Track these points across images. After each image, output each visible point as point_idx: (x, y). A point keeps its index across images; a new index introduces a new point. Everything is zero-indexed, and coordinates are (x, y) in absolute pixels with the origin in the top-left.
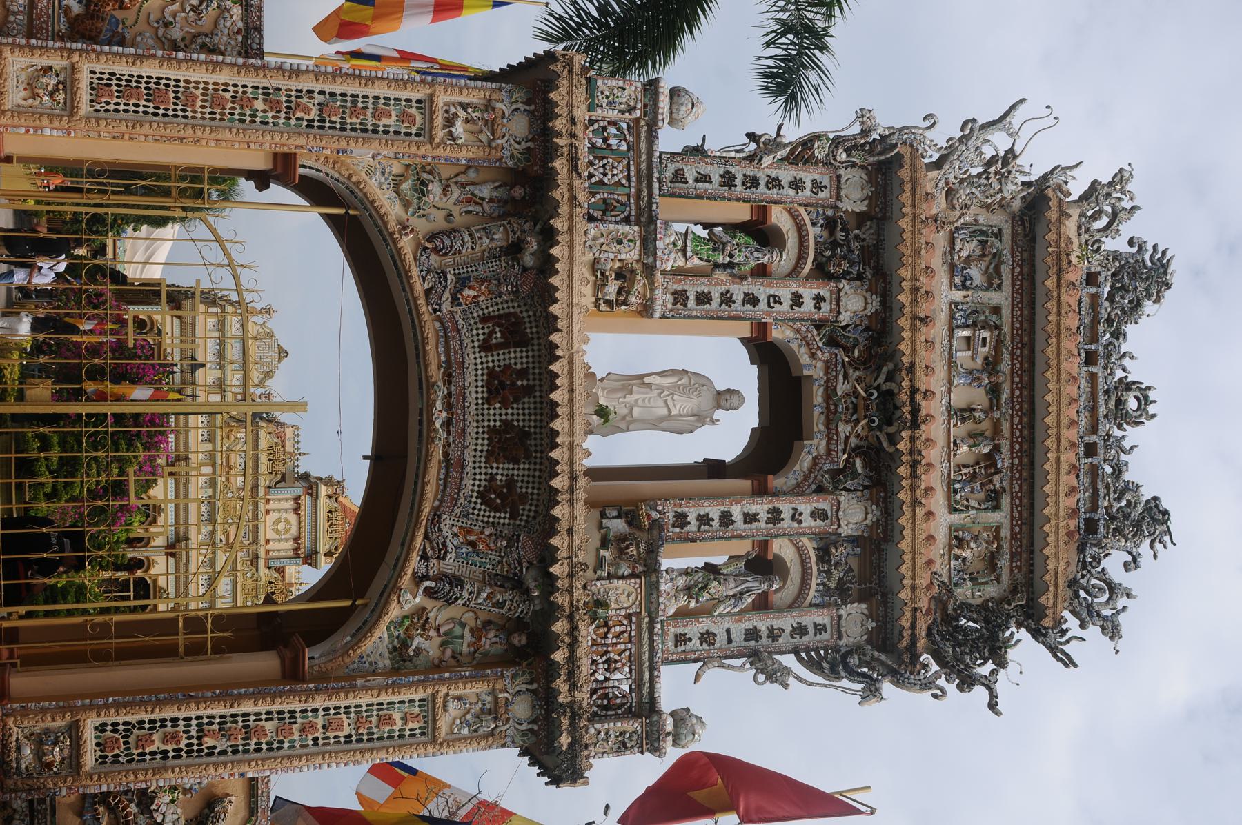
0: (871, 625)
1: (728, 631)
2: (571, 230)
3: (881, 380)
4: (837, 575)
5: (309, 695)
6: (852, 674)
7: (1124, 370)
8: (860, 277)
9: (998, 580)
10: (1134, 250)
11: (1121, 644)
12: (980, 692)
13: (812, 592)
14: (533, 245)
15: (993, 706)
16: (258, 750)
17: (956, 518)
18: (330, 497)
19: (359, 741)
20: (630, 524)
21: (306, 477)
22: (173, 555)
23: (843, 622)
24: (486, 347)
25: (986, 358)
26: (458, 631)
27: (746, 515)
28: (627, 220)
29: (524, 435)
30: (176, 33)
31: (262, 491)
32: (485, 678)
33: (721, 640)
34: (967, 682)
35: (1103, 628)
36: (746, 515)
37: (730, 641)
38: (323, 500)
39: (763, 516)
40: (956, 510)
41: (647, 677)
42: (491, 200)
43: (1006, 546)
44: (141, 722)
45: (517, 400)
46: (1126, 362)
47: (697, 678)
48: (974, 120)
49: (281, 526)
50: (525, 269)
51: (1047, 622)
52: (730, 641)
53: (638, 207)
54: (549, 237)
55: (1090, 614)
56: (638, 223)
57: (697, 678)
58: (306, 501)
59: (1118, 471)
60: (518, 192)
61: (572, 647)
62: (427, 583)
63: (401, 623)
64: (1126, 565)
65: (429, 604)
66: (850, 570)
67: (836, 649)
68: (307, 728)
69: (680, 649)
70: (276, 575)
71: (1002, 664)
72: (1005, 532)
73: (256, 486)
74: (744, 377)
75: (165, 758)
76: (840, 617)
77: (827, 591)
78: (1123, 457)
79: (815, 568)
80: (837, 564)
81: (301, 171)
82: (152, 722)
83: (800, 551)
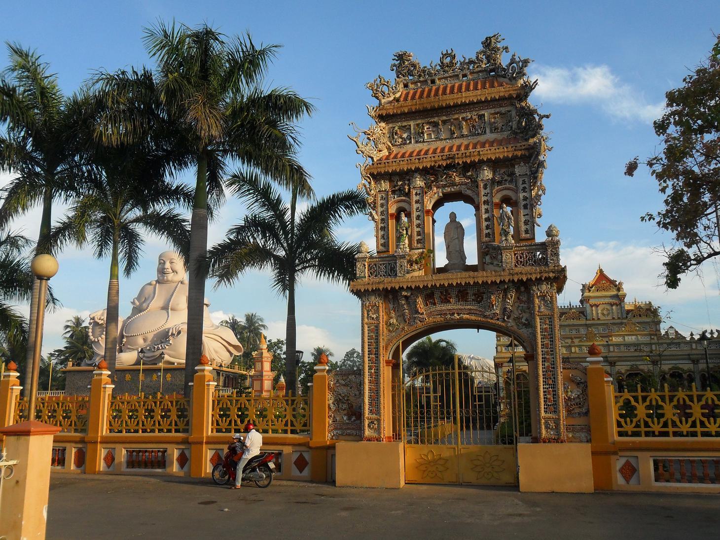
0: (522, 164)
1: (524, 215)
2: (399, 283)
3: (441, 170)
4: (506, 177)
5: (537, 353)
6: (537, 171)
7: (436, 65)
8: (409, 180)
9: (509, 111)
10: (395, 68)
11: (531, 58)
12: (544, 121)
13: (511, 186)
14: (404, 293)
15: (547, 117)
16: (554, 368)
17: (488, 130)
18: (590, 291)
19: (552, 337)
20: (487, 255)
21: (582, 302)
22: (615, 363)
23: (521, 174)
24: (435, 304)
25: (434, 126)
26: (520, 308)
27: (486, 213)
28: (396, 263)
29: (459, 291)
30: (357, 393)
31: (588, 322)
32: (533, 299)
33: (527, 218)
34: (540, 127)
35: (526, 66)
36: (486, 213)
37: (527, 215)
38: (591, 294)
39: (486, 207)
40: (485, 132)
41: (534, 247)
42: (394, 304)
43: (497, 110)
44: (544, 401)
45: (449, 294)
46: (433, 65)
47: (539, 226)
48: (356, 151)
49: (605, 312)
50: (412, 294)
51: (522, 92)
52: (527, 215)
53: (391, 260)
54: (401, 289)
55: (521, 72)
56: (396, 260)
57: (539, 226)
58: (592, 301)
59: (471, 62)
60: (391, 297)
61: (521, 273)
62: (505, 318)
63: (518, 325)
64: (506, 52)
65: (512, 317)
66: (504, 172)
67: (530, 175)
68: (547, 353)
69: (530, 232)
70: (630, 314)
71: (535, 111)
72: (492, 111)
73: (586, 325)
74: (449, 207)
75: (555, 395)
76: (519, 175)
77: (511, 182)
78: (467, 61)
79: (503, 186)
80: (502, 178)
81: (390, 359)
82: (544, 398)
83: (498, 191)
